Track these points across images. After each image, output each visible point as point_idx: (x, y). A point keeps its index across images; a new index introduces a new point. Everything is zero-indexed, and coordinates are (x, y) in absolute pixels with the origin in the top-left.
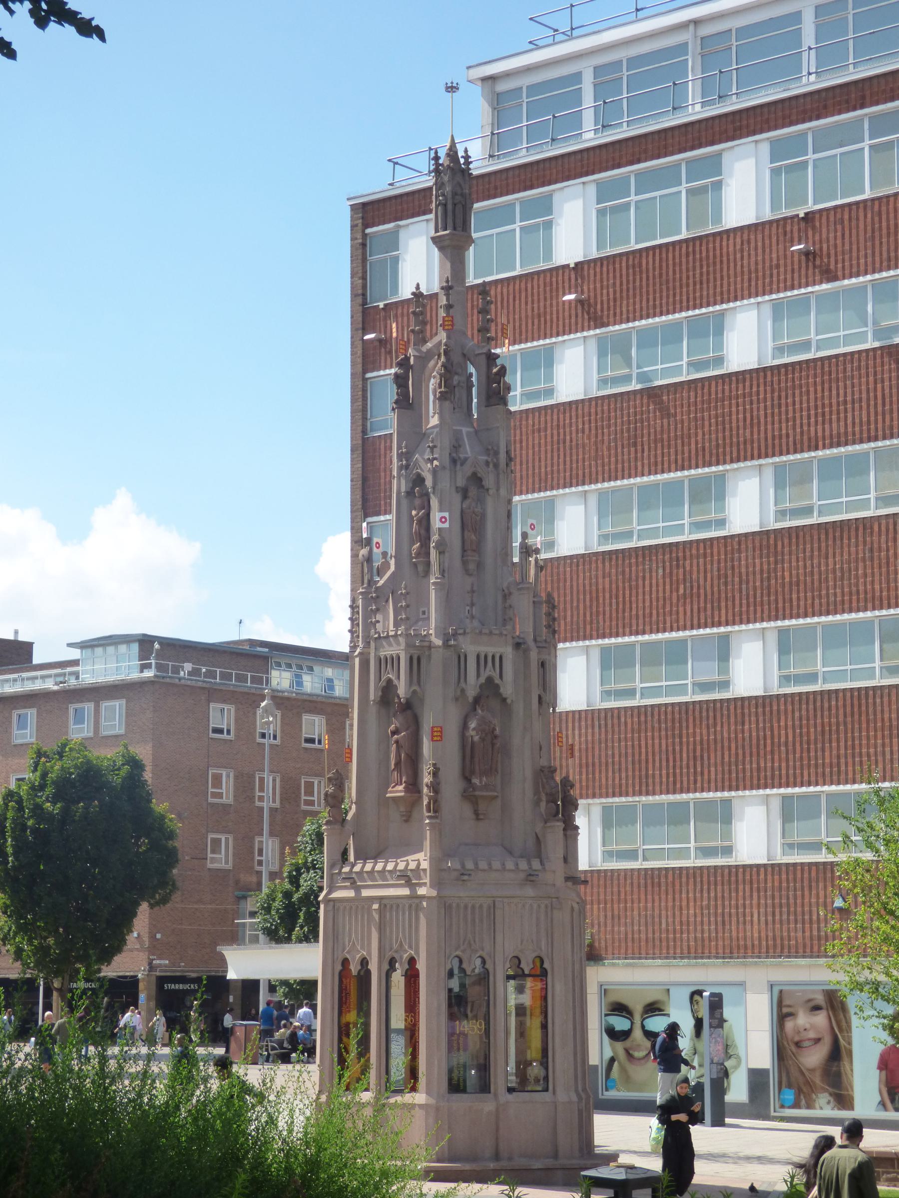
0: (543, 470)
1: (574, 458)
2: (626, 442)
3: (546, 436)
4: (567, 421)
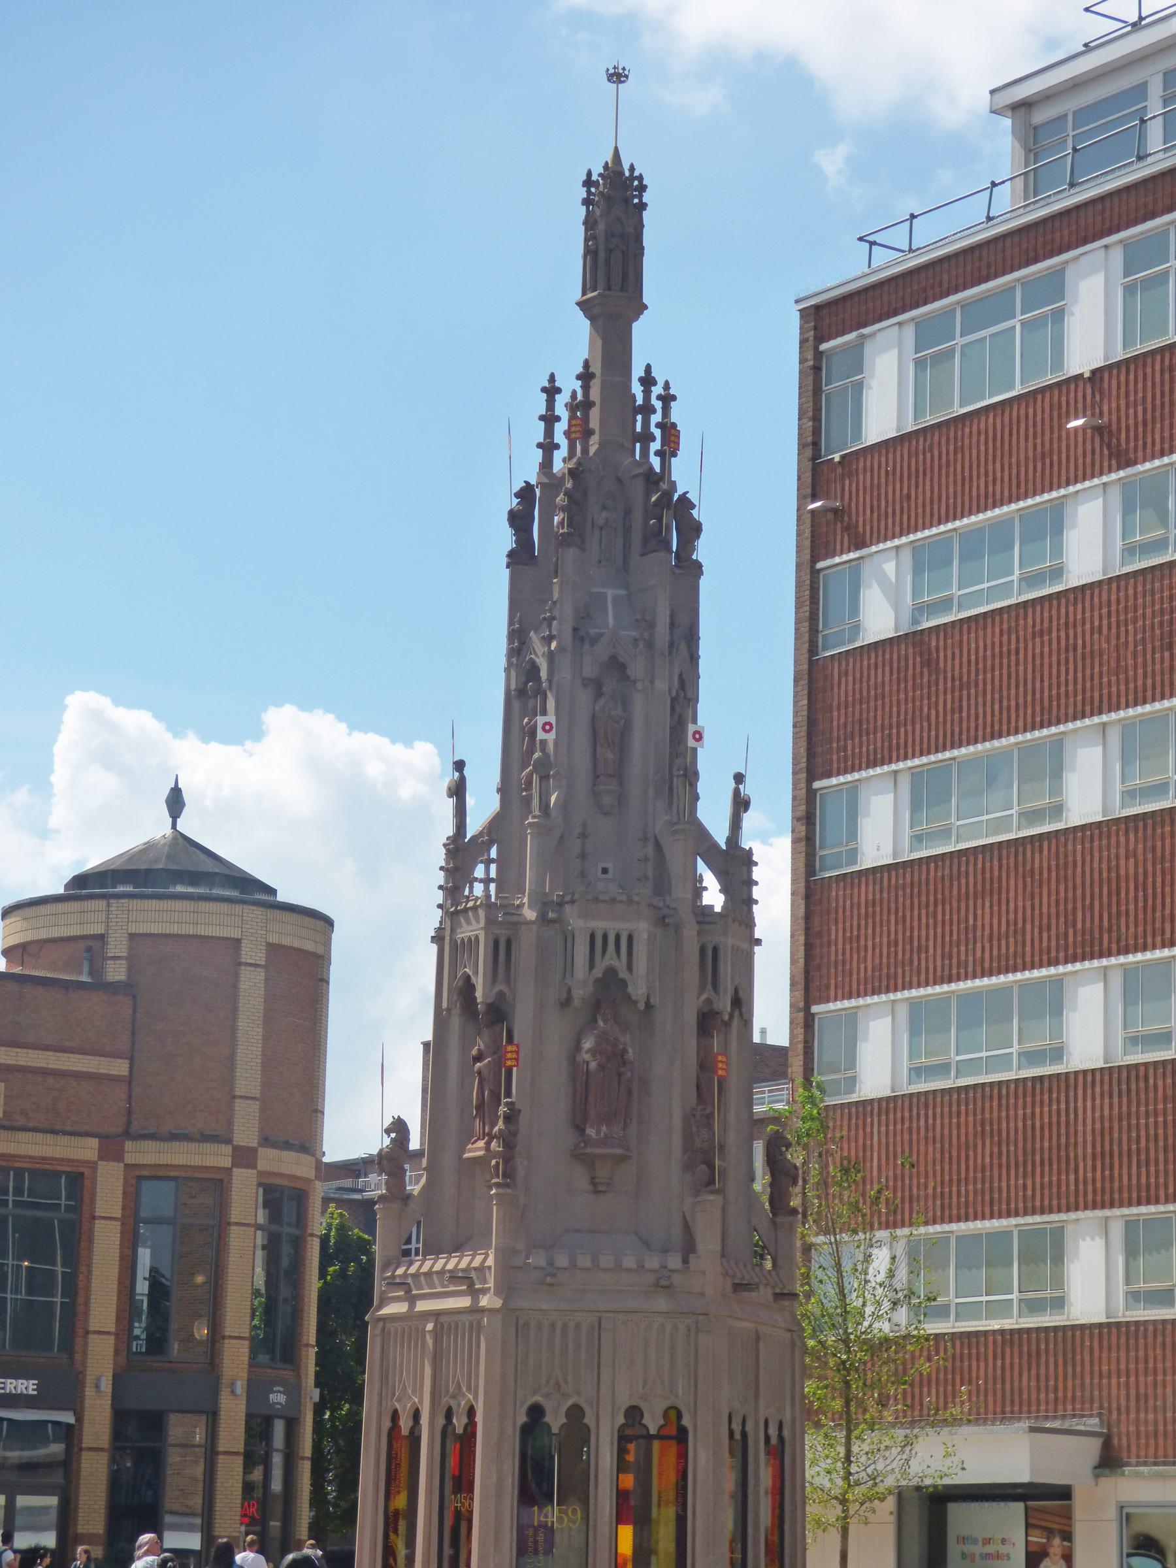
0: (1046, 694)
1: (1088, 672)
2: (1157, 644)
3: (1050, 640)
4: (1079, 617)
